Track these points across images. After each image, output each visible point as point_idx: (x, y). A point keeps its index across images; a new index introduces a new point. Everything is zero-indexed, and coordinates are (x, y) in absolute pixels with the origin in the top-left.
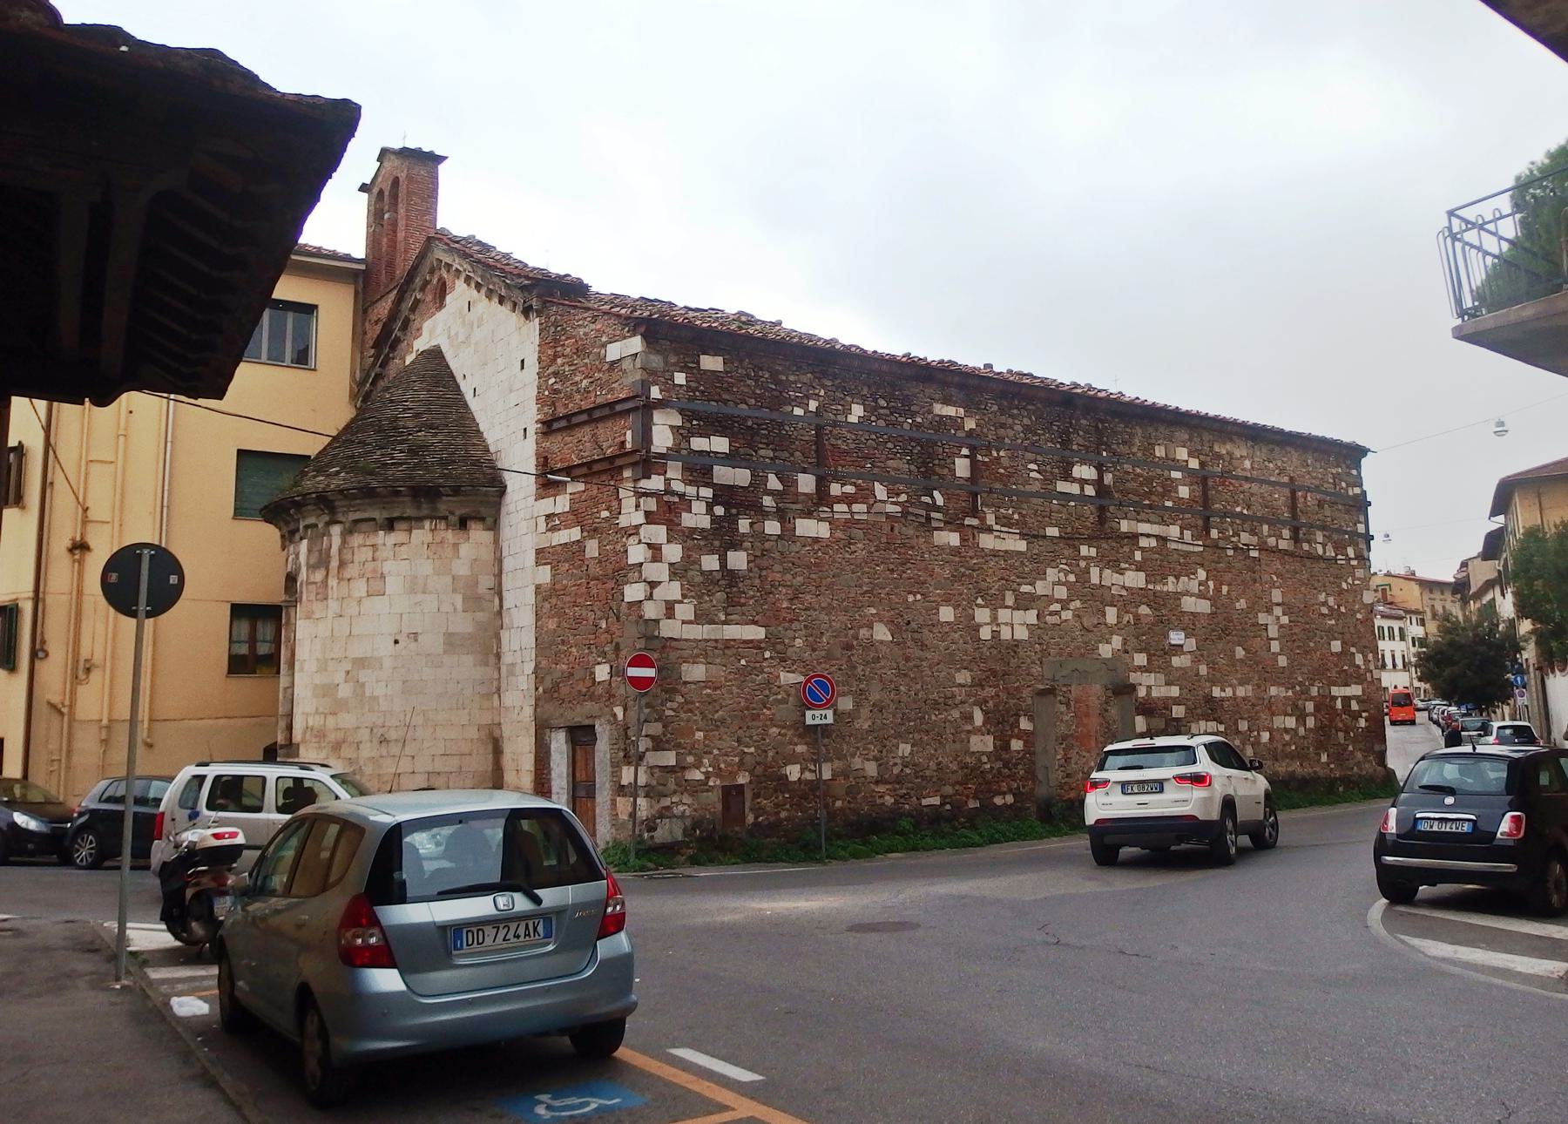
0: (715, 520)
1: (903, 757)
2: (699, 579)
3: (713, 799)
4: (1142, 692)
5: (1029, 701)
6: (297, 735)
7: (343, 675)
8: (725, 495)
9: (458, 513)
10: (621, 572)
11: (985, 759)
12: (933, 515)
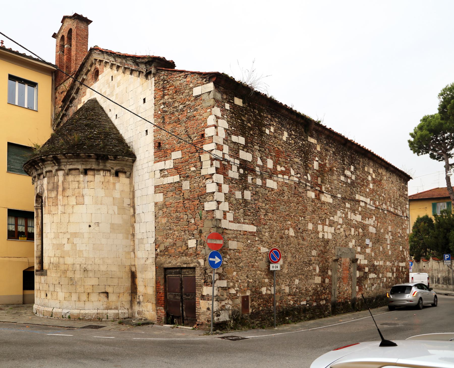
0: (240, 175)
1: (296, 285)
2: (235, 202)
3: (239, 301)
4: (358, 262)
5: (331, 263)
6: (46, 266)
7: (66, 240)
8: (244, 165)
9: (115, 169)
10: (203, 196)
11: (318, 286)
12: (308, 184)
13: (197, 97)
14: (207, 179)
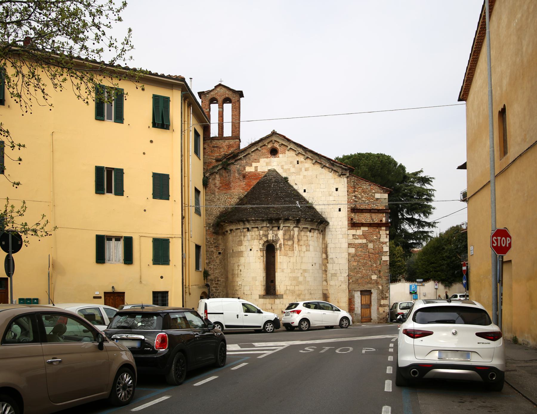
7: (300, 274)
13: (377, 199)
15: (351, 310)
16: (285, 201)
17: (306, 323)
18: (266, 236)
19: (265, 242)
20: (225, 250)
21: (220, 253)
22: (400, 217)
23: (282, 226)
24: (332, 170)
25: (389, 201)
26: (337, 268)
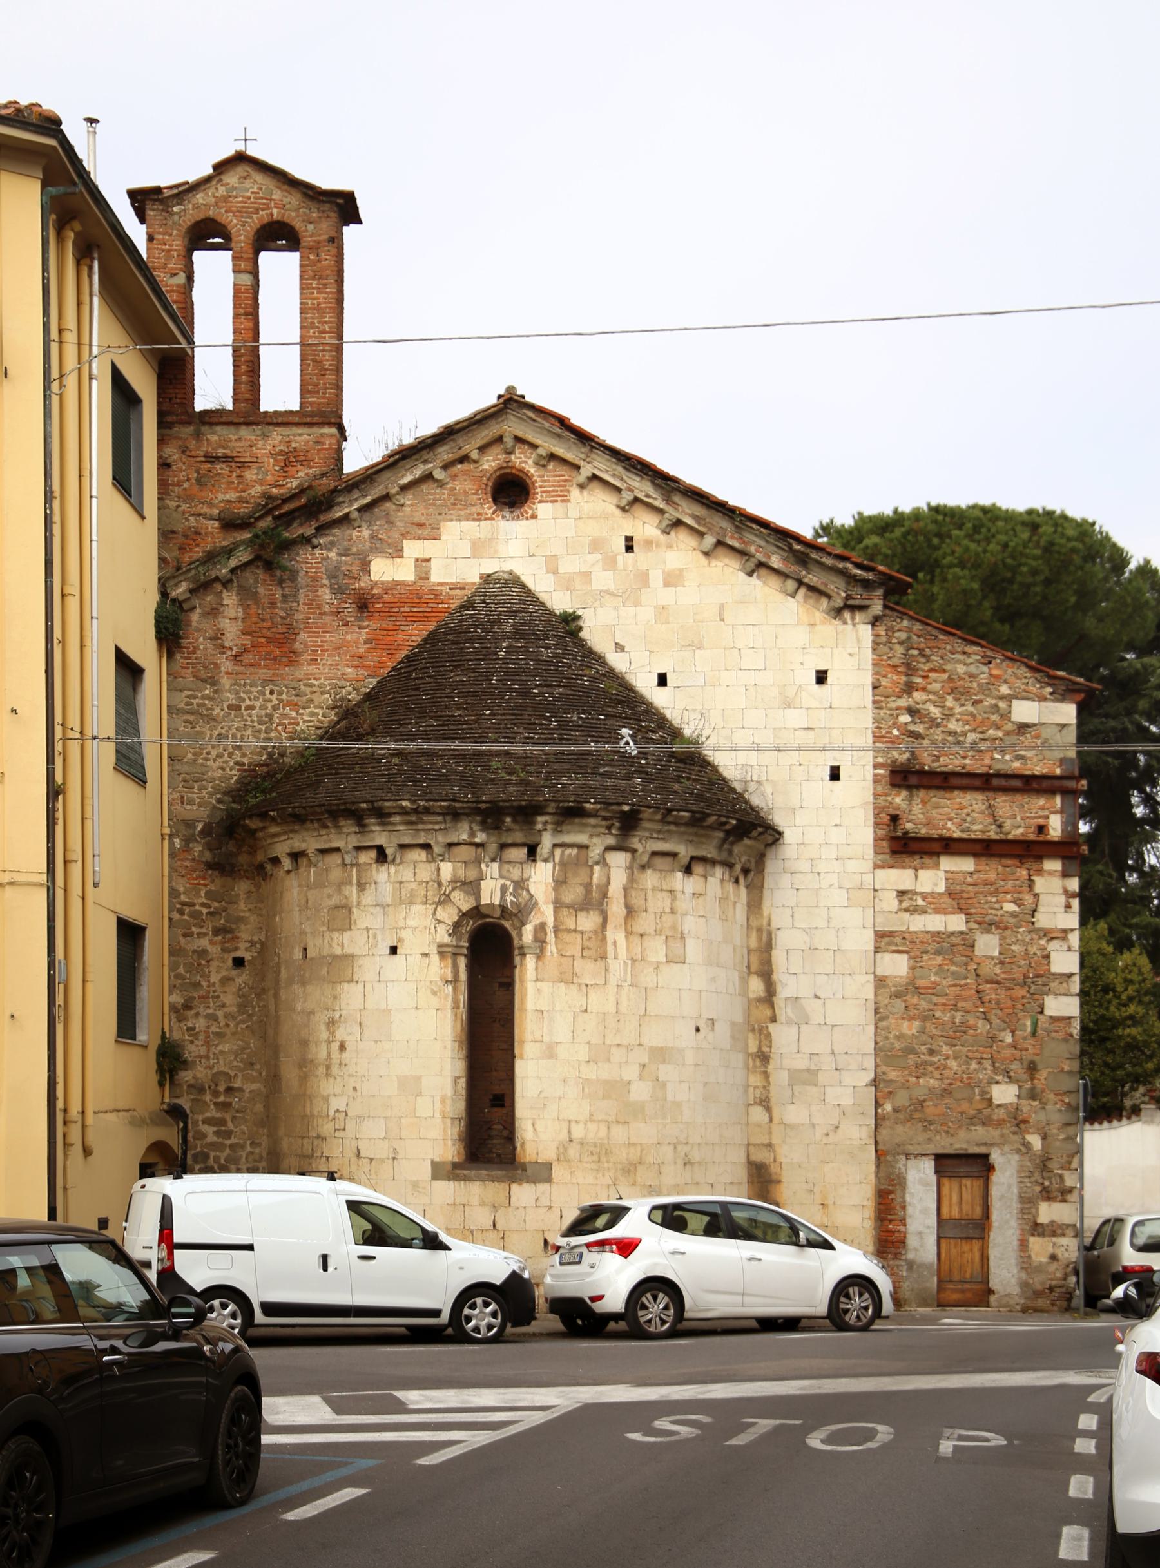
13: (1023, 727)
14: (1052, 938)
15: (888, 1243)
16: (564, 725)
17: (663, 1299)
18: (472, 886)
19: (464, 915)
20: (266, 948)
21: (239, 962)
22: (1139, 811)
23: (547, 841)
24: (800, 583)
25: (1082, 738)
26: (822, 1047)
